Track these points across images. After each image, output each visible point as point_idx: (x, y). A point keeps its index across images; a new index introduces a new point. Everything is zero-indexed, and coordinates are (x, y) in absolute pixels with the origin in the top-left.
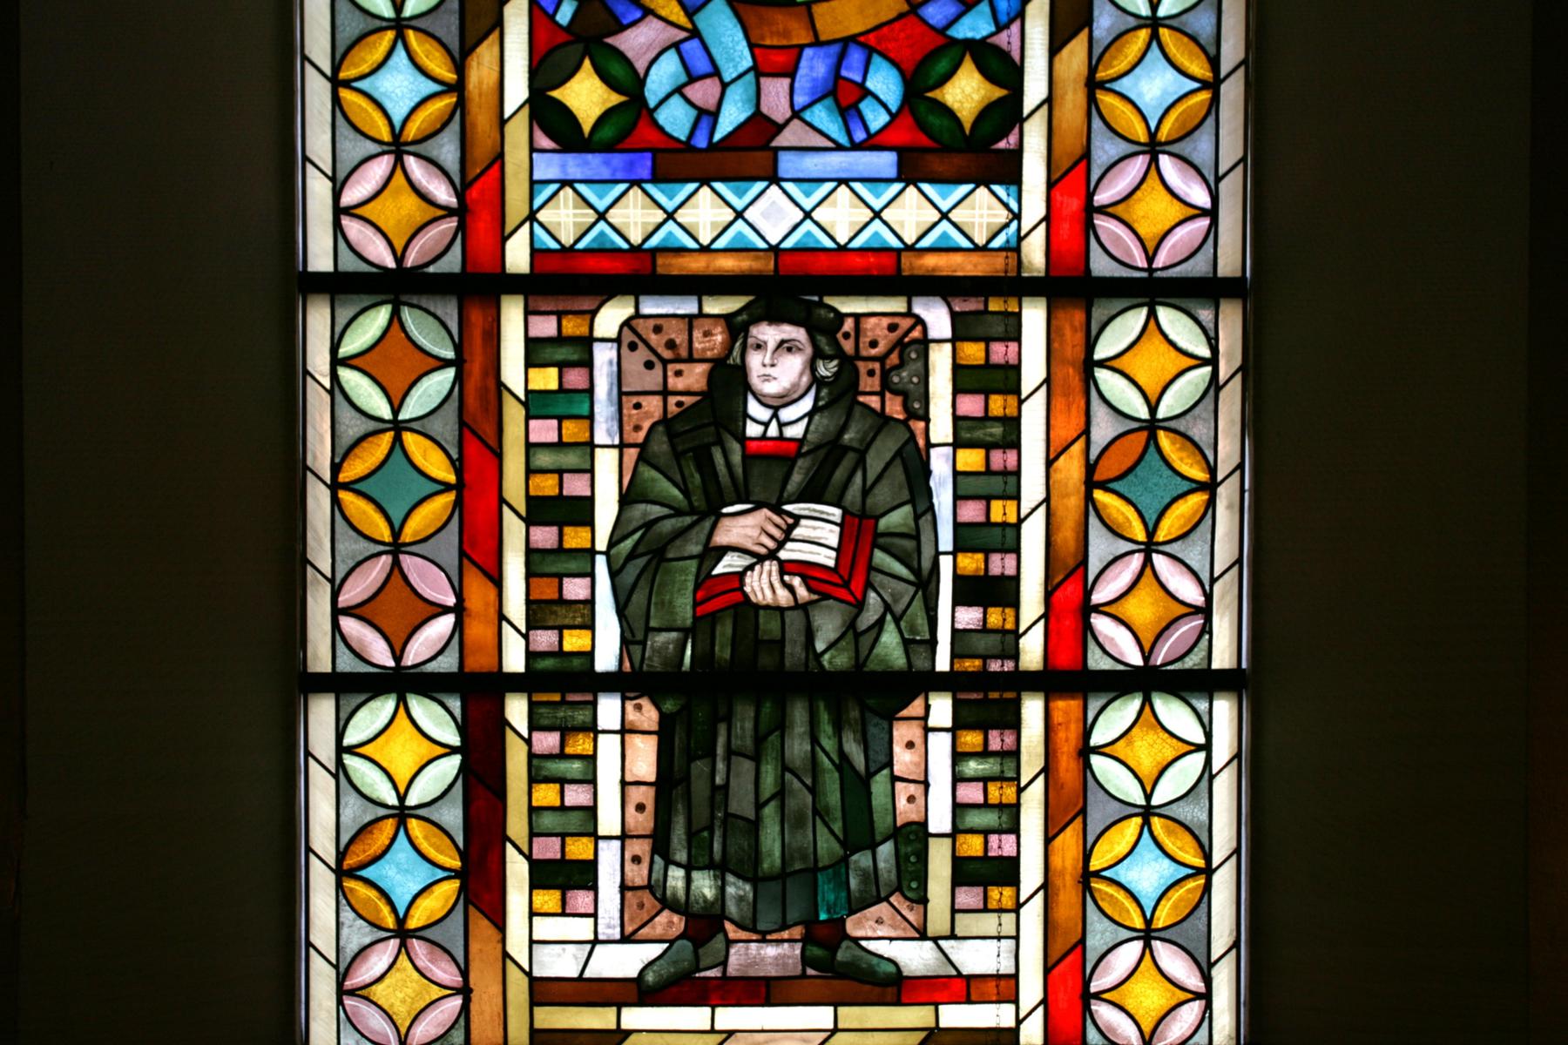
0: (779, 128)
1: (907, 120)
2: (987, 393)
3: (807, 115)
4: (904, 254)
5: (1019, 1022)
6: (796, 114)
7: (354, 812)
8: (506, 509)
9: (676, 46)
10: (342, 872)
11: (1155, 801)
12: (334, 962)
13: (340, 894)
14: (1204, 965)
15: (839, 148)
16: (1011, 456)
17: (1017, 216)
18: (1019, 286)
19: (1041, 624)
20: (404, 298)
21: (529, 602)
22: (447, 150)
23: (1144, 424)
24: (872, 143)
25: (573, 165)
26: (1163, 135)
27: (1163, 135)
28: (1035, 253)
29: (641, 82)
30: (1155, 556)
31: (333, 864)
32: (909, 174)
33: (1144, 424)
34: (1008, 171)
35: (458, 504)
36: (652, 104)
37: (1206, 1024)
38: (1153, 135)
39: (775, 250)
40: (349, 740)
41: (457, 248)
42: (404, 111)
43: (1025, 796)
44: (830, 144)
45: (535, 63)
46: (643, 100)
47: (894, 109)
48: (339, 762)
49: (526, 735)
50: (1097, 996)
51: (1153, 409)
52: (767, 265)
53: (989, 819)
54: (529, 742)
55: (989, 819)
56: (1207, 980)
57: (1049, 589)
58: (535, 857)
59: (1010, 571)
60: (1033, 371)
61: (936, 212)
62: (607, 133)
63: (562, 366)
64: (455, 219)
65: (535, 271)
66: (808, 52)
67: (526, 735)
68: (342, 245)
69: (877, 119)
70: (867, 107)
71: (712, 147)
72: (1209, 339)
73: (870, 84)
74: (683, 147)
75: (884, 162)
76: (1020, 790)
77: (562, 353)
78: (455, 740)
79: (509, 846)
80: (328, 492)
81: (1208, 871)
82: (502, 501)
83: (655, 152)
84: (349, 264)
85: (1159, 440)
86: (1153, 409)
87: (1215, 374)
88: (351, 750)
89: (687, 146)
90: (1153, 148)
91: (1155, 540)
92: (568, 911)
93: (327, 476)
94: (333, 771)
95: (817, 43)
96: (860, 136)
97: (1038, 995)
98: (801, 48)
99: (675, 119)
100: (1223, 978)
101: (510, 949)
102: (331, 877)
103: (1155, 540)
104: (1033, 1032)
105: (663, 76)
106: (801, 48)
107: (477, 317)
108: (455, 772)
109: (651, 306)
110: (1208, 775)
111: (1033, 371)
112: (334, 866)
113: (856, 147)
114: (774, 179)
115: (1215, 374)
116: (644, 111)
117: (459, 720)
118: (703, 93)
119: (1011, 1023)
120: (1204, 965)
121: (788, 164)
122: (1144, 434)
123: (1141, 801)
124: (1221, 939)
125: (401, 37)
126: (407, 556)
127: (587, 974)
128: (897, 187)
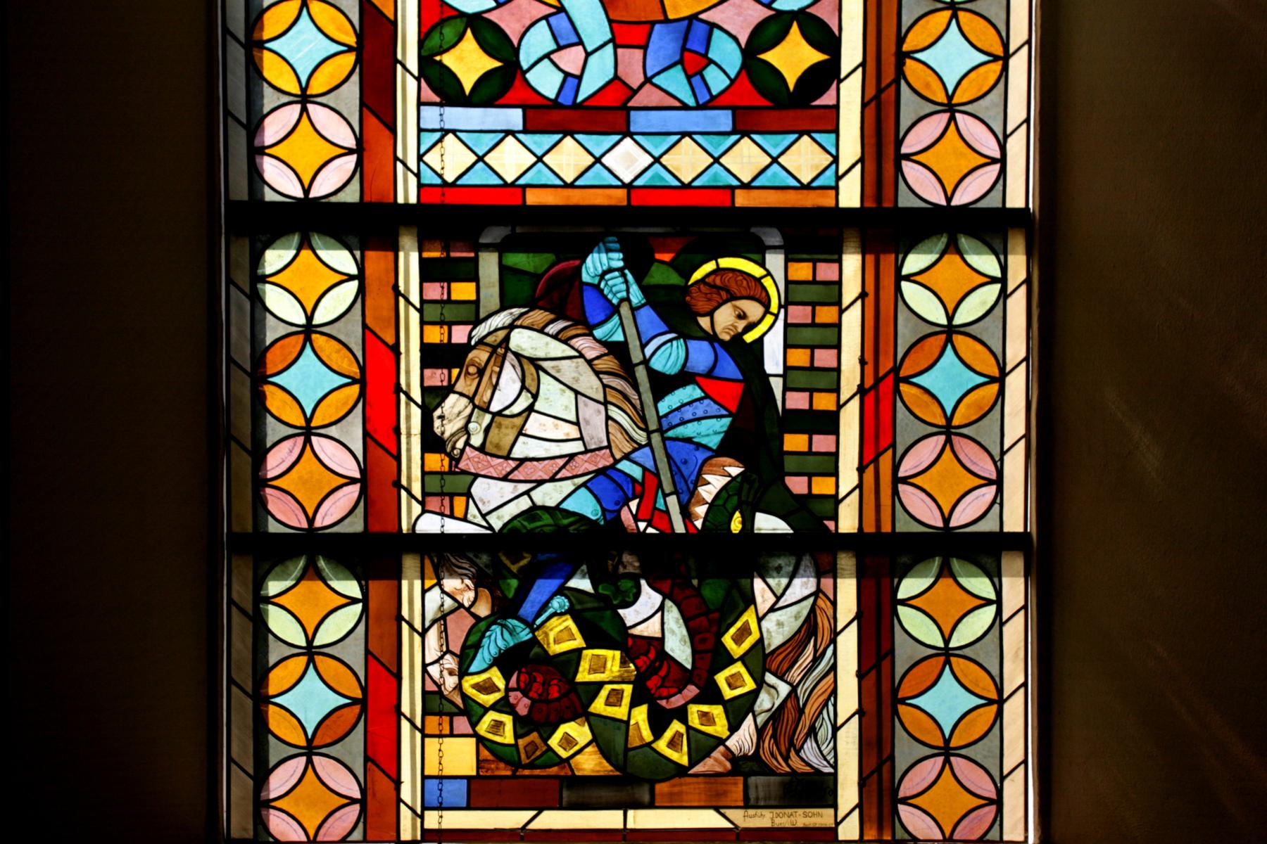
0: (635, 92)
1: (745, 82)
2: (811, 432)
3: (655, 80)
4: (738, 192)
5: (837, 824)
6: (648, 80)
8: (402, 805)
9: (546, 18)
11: (958, 320)
14: (1001, 137)
15: (685, 107)
17: (836, 160)
24: (712, 103)
25: (457, 116)
28: (850, 195)
29: (516, 51)
32: (742, 129)
34: (830, 121)
35: (363, 492)
36: (525, 66)
37: (1001, 182)
39: (629, 187)
41: (355, 184)
43: (845, 316)
44: (678, 104)
45: (422, 37)
46: (517, 63)
47: (733, 76)
50: (908, 157)
52: (619, 197)
53: (813, 293)
54: (418, 175)
56: (1003, 148)
60: (851, 289)
62: (485, 93)
65: (423, 201)
66: (657, 27)
69: (717, 81)
70: (712, 74)
71: (575, 106)
72: (995, 463)
73: (710, 55)
74: (550, 103)
75: (723, 120)
76: (841, 312)
77: (449, 312)
80: (242, 51)
81: (1005, 58)
83: (525, 108)
85: (953, 567)
86: (950, 318)
87: (999, 612)
89: (554, 104)
90: (951, 108)
92: (455, 732)
93: (241, 36)
95: (666, 21)
96: (704, 98)
97: (855, 800)
98: (653, 23)
99: (546, 81)
100: (1017, 147)
104: (850, 829)
105: (537, 42)
106: (653, 23)
107: (378, 588)
110: (999, 622)
111: (851, 289)
113: (699, 107)
114: (627, 133)
115: (999, 612)
116: (519, 71)
118: (571, 59)
119: (833, 408)
120: (1001, 137)
121: (639, 121)
122: (943, 337)
123: (944, 321)
124: (1017, 112)
126: (318, 336)
128: (734, 138)
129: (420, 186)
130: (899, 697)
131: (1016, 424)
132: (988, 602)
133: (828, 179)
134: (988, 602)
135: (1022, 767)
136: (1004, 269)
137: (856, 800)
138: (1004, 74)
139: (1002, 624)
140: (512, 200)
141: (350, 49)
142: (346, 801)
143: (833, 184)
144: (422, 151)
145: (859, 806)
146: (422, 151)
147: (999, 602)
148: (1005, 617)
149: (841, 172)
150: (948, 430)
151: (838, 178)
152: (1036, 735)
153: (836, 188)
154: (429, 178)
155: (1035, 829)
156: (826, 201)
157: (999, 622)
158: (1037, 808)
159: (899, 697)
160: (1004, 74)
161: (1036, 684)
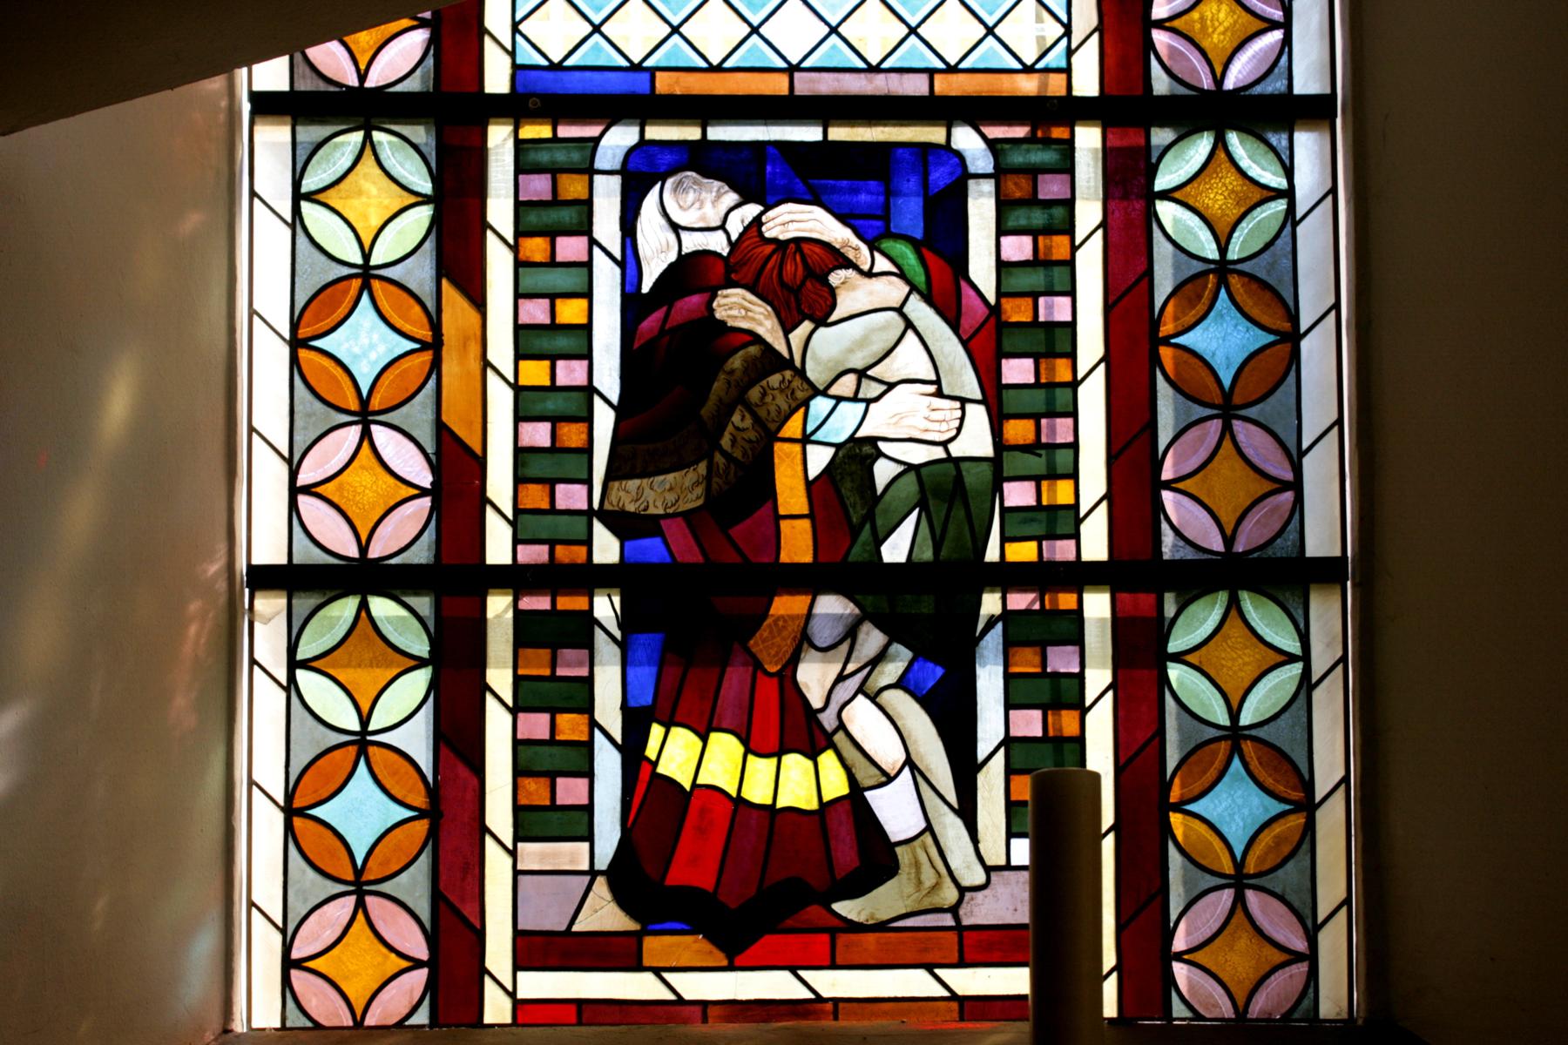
7: (311, 741)
10: (291, 811)
12: (280, 924)
13: (290, 839)
16: (1063, 425)
18: (1074, 110)
19: (1100, 233)
20: (374, 121)
21: (518, 810)
22: (419, 414)
23: (1212, 266)
26: (1251, 867)
27: (1251, 867)
30: (1228, 723)
31: (287, 336)
33: (1212, 266)
37: (1308, 839)
38: (1239, 865)
40: (308, 185)
42: (376, 222)
48: (292, 678)
49: (510, 846)
51: (1234, 714)
55: (1035, 279)
57: (1110, 302)
58: (520, 995)
59: (1063, 315)
61: (982, 27)
63: (555, 420)
64: (430, 352)
67: (510, 846)
68: (302, 239)
78: (426, 187)
79: (487, 980)
82: (485, 830)
84: (306, 554)
87: (1307, 672)
88: (311, 197)
91: (1229, 742)
94: (289, 220)
101: (492, 356)
102: (279, 818)
103: (1229, 742)
108: (421, 989)
109: (656, 132)
112: (282, 803)
115: (1307, 672)
117: (432, 630)
125: (364, 403)
127: (575, 928)
129: (517, 68)
130: (1161, 335)
131: (1332, 883)
132: (1290, 658)
133: (1056, 58)
134: (1290, 658)
135: (1336, 430)
136: (1304, 638)
137: (1094, 22)
138: (1287, 49)
139: (1295, 224)
140: (639, 83)
141: (424, 200)
142: (415, 492)
143: (1063, 64)
144: (518, 18)
145: (1103, 225)
146: (518, 18)
147: (1306, 657)
148: (1299, 214)
149: (1074, 46)
150: (1239, 881)
151: (1070, 52)
152: (1358, 742)
153: (1068, 71)
154: (527, 56)
155: (1348, 202)
156: (1056, 86)
157: (1307, 684)
158: (1353, 251)
159: (1161, 335)
160: (1287, 49)
161: (1360, 883)
